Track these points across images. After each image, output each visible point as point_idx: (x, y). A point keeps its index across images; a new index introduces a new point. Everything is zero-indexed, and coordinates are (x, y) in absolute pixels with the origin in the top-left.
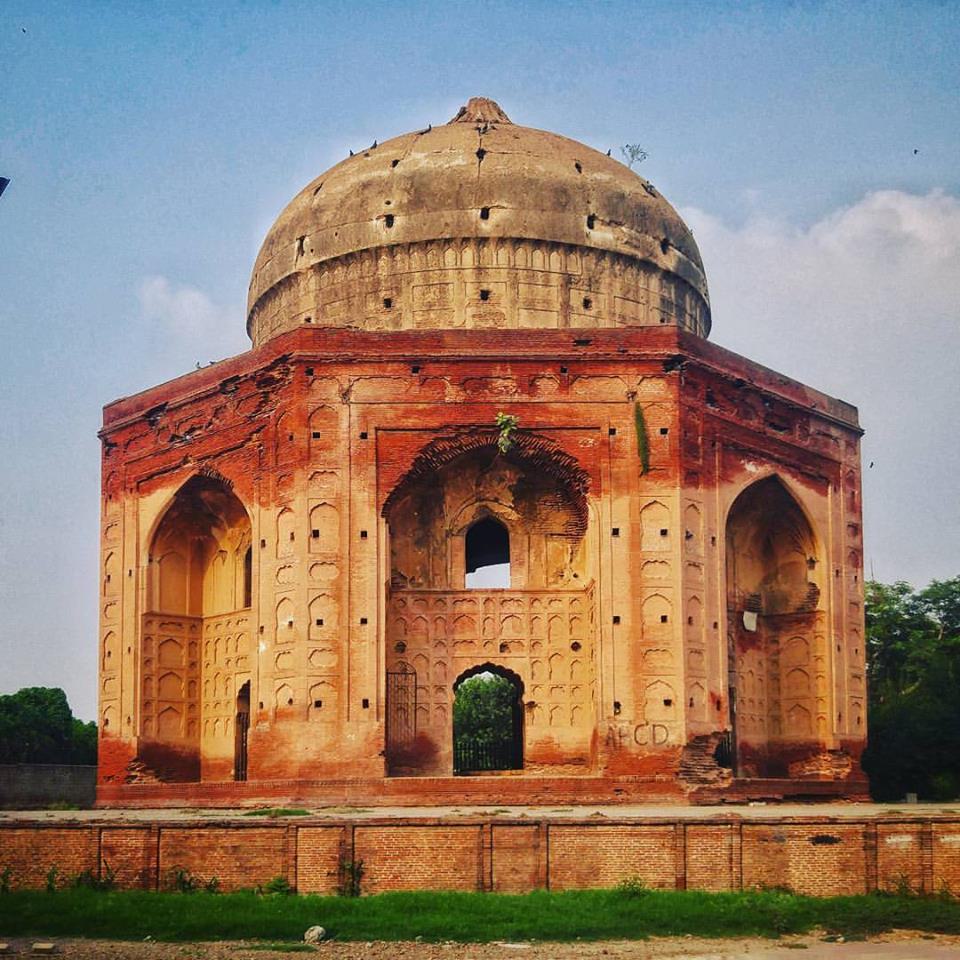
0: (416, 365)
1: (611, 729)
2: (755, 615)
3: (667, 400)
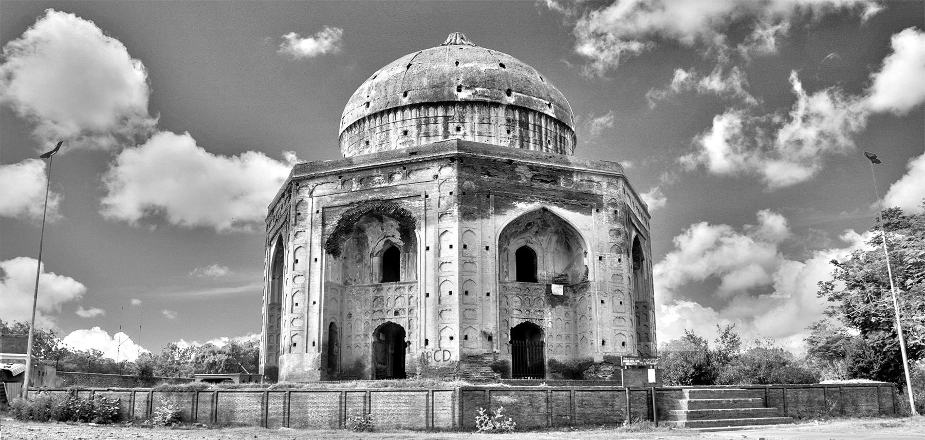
0: (340, 175)
2: (562, 286)
3: (452, 177)
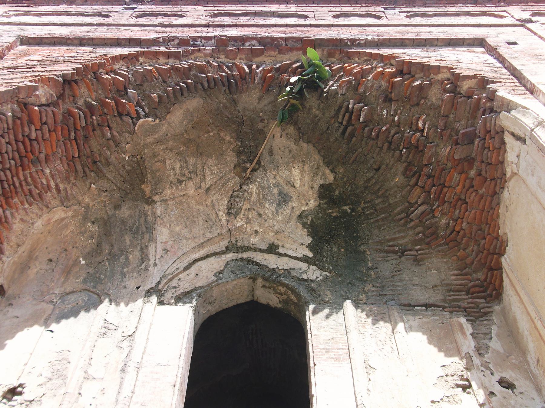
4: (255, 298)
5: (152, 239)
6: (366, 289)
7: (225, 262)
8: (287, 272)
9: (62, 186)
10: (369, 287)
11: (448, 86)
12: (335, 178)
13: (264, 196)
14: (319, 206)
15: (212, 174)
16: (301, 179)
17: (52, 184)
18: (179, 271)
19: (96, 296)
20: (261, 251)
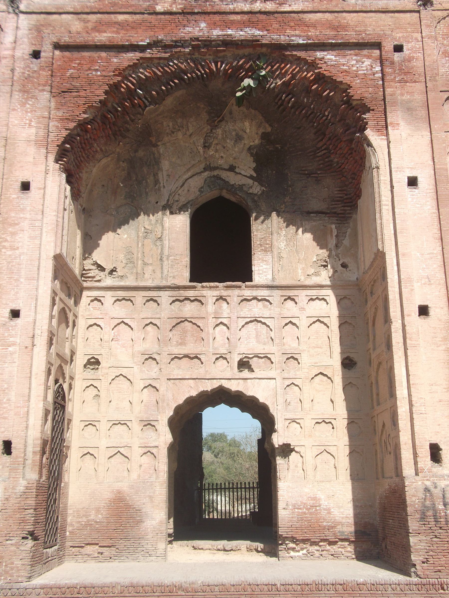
1: (427, 490)
4: (222, 195)
5: (160, 169)
6: (286, 200)
7: (204, 179)
8: (241, 187)
9: (103, 148)
10: (287, 199)
11: (345, 98)
12: (272, 130)
13: (226, 136)
14: (261, 143)
15: (193, 126)
16: (250, 129)
17: (98, 149)
18: (178, 189)
19: (135, 208)
20: (225, 170)
